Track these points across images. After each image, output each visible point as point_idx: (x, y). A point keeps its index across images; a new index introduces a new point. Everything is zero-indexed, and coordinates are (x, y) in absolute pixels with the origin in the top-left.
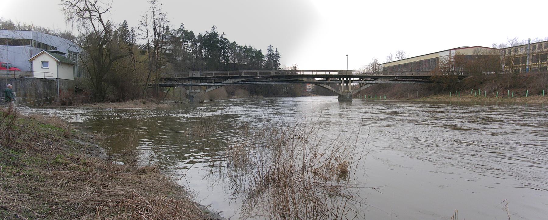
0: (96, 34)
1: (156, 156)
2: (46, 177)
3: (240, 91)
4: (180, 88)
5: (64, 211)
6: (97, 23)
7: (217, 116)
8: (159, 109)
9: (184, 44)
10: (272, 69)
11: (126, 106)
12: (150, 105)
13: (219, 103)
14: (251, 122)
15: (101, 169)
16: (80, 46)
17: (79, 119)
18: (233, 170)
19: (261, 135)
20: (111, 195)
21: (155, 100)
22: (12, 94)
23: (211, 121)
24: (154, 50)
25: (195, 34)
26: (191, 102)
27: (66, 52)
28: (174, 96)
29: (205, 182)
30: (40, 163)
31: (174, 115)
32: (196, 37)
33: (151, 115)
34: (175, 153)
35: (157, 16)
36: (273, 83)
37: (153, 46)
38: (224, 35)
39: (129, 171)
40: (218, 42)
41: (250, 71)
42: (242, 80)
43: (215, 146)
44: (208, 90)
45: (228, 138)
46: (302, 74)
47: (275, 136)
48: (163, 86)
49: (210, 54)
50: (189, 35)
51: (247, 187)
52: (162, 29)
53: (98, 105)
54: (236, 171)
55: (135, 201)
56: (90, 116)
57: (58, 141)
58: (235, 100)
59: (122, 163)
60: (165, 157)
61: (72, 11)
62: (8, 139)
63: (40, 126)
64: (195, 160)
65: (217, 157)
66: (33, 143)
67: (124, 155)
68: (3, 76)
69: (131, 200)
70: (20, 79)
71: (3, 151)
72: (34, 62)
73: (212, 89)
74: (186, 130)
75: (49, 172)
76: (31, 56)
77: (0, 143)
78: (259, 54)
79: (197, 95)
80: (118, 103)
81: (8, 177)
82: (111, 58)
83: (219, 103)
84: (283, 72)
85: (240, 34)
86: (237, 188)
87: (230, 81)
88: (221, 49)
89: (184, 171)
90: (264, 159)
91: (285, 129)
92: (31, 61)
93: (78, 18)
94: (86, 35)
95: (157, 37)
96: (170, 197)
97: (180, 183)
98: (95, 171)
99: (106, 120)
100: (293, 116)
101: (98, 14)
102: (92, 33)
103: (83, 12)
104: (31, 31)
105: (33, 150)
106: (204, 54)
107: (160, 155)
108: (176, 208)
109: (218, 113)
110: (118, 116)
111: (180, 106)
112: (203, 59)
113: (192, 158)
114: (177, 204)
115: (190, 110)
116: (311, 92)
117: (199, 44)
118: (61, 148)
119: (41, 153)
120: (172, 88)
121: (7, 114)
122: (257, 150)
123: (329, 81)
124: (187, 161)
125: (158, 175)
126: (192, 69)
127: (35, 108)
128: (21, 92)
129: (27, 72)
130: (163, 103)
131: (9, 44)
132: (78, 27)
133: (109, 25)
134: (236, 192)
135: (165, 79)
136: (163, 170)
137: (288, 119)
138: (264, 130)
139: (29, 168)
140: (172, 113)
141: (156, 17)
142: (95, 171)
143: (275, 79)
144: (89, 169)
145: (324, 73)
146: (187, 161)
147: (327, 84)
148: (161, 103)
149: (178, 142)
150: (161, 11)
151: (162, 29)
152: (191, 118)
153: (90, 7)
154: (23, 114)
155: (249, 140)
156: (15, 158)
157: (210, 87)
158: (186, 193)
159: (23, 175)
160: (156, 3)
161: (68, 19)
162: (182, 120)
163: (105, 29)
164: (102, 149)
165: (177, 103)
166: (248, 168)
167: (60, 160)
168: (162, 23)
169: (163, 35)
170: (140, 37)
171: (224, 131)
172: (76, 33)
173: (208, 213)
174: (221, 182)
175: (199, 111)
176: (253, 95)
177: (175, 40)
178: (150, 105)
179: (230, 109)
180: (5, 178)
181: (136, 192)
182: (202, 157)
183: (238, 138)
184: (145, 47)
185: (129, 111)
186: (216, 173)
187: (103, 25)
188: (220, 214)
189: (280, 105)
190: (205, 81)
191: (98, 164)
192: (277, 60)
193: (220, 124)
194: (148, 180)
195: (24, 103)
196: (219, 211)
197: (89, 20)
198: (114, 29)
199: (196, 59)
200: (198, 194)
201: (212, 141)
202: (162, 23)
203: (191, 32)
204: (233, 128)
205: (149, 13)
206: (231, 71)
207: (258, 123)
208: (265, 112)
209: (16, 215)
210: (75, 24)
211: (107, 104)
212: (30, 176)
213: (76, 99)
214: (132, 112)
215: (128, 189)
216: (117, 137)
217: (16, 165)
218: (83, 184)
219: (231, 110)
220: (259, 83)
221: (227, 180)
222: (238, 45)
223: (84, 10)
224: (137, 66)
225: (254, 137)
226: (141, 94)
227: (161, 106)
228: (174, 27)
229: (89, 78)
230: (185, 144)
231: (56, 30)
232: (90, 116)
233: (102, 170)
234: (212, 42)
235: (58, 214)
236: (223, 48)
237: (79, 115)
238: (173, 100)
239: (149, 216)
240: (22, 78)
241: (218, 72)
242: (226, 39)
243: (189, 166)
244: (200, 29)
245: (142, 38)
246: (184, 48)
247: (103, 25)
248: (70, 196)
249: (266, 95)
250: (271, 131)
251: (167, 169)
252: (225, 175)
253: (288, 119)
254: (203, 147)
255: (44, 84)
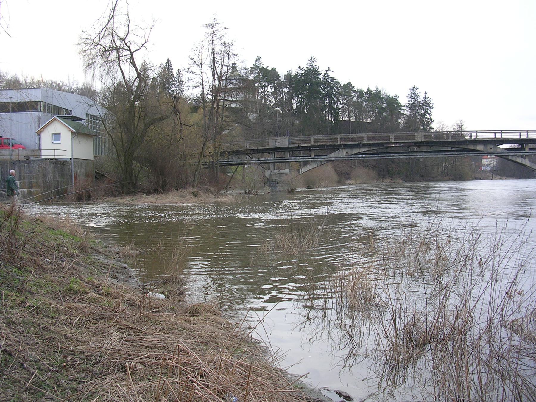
0: (126, 84)
1: (214, 287)
2: (57, 311)
3: (360, 171)
4: (254, 167)
5: (82, 366)
6: (127, 67)
7: (319, 217)
8: (218, 204)
9: (261, 90)
10: (417, 130)
11: (167, 200)
12: (204, 197)
13: (322, 193)
14: (381, 228)
15: (131, 304)
16: (103, 105)
17: (99, 222)
18: (347, 316)
19: (398, 253)
20: (147, 347)
21: (212, 189)
22: (15, 184)
23: (308, 226)
24: (213, 105)
25: (279, 73)
26: (273, 192)
27: (84, 117)
28: (243, 181)
29: (297, 334)
30: (49, 289)
31: (243, 216)
32: (282, 78)
33: (206, 214)
34: (246, 283)
35: (219, 48)
36: (419, 156)
37: (210, 97)
38: (330, 73)
39: (173, 309)
40: (319, 84)
41: (377, 134)
42: (363, 150)
43: (316, 272)
44: (303, 170)
45: (338, 257)
46: (474, 137)
47: (424, 253)
48: (225, 165)
49: (306, 105)
50: (269, 76)
51: (371, 346)
52: (225, 69)
53: (127, 199)
54: (352, 317)
55: (183, 359)
56: (115, 217)
57: (72, 256)
58: (351, 188)
59: (162, 296)
60: (230, 288)
61: (94, 52)
62: (11, 252)
63: (49, 233)
64: (280, 296)
65: (318, 292)
66: (40, 258)
67: (165, 283)
68: (5, 157)
69: (176, 357)
70: (25, 162)
71: (4, 269)
72: (43, 135)
73: (309, 167)
74: (264, 242)
75: (62, 305)
76: (39, 126)
77: (2, 258)
78: (393, 103)
79: (284, 178)
80: (156, 196)
81: (11, 308)
82: (147, 121)
83: (322, 193)
84: (438, 134)
85: (365, 66)
86: (353, 348)
87: (342, 153)
88: (325, 97)
89: (261, 313)
90: (403, 297)
91: (442, 241)
92: (39, 134)
93: (101, 62)
94: (112, 88)
95: (217, 82)
96: (239, 358)
97: (254, 335)
98: (123, 306)
99: (138, 224)
100: (458, 218)
101: (129, 53)
102: (120, 84)
103: (108, 53)
104: (40, 88)
105: (41, 269)
106: (295, 106)
107: (221, 285)
108: (249, 376)
109: (321, 211)
110: (155, 217)
111: (254, 199)
112: (293, 115)
113: (274, 293)
114: (250, 369)
115: (271, 205)
116: (490, 171)
117: (286, 90)
118: (77, 267)
119: (50, 274)
120: (240, 168)
121: (9, 215)
122: (391, 281)
123: (527, 150)
124: (267, 297)
125: (218, 318)
126: (273, 133)
127: (42, 205)
128: (26, 180)
129: (33, 150)
130: (225, 195)
131: (14, 111)
132: (101, 76)
133: (145, 69)
134: (353, 355)
135: (229, 153)
136: (226, 310)
137: (448, 223)
138: (404, 243)
139: (36, 296)
140: (240, 212)
141: (216, 50)
142: (123, 306)
143: (424, 148)
144: (114, 302)
145: (516, 136)
146: (267, 297)
147: (522, 156)
148: (222, 195)
149: (251, 264)
150: (224, 39)
151: (225, 69)
152: (272, 222)
153: (118, 43)
154: (28, 214)
155: (377, 261)
156: (19, 280)
157: (306, 163)
158: (265, 351)
159: (30, 306)
160: (217, 26)
161: (88, 66)
162: (258, 225)
163: (139, 76)
164: (133, 272)
165: (249, 193)
166: (374, 312)
167: (75, 286)
168: (226, 59)
169: (226, 79)
170: (191, 84)
171: (332, 244)
172: (98, 86)
173: (302, 388)
174: (325, 336)
175: (288, 209)
176: (384, 178)
177: (246, 85)
178: (204, 197)
179: (343, 205)
180: (8, 309)
181: (184, 345)
182: (292, 290)
183: (356, 257)
184: (198, 101)
185: (172, 208)
186: (317, 320)
187: (136, 70)
188: (323, 392)
189: (433, 196)
190: (297, 153)
191: (128, 296)
192: (426, 113)
193: (325, 232)
194: (203, 326)
195: (30, 197)
196: (321, 386)
197: (116, 63)
198: (152, 75)
199: (282, 116)
200: (284, 356)
201: (310, 262)
202: (226, 59)
203: (274, 70)
204: (347, 239)
205: (206, 43)
206: (344, 135)
207: (393, 231)
208: (405, 210)
209: (22, 364)
210: (97, 73)
211: (139, 197)
212: (37, 308)
213: (95, 191)
214: (176, 211)
215: (171, 338)
216: (154, 251)
217: (20, 291)
218: (107, 325)
219: (344, 206)
220: (395, 157)
221: (336, 333)
222: (355, 89)
223: (110, 50)
224: (185, 132)
225: (385, 257)
226: (191, 179)
227: (222, 199)
228: (245, 62)
229: (115, 156)
230: (262, 267)
231: (71, 84)
232: (115, 217)
233: (133, 305)
234: (310, 85)
235: (75, 368)
236: (329, 95)
237: (100, 215)
238: (242, 188)
239: (205, 385)
240: (27, 160)
241: (320, 137)
242: (333, 79)
243: (270, 305)
244: (287, 63)
245: (195, 85)
246: (262, 97)
247: (136, 70)
248: (90, 343)
249: (408, 178)
250: (417, 245)
251: (232, 310)
252: (332, 324)
253: (448, 223)
254: (294, 273)
255: (55, 167)
